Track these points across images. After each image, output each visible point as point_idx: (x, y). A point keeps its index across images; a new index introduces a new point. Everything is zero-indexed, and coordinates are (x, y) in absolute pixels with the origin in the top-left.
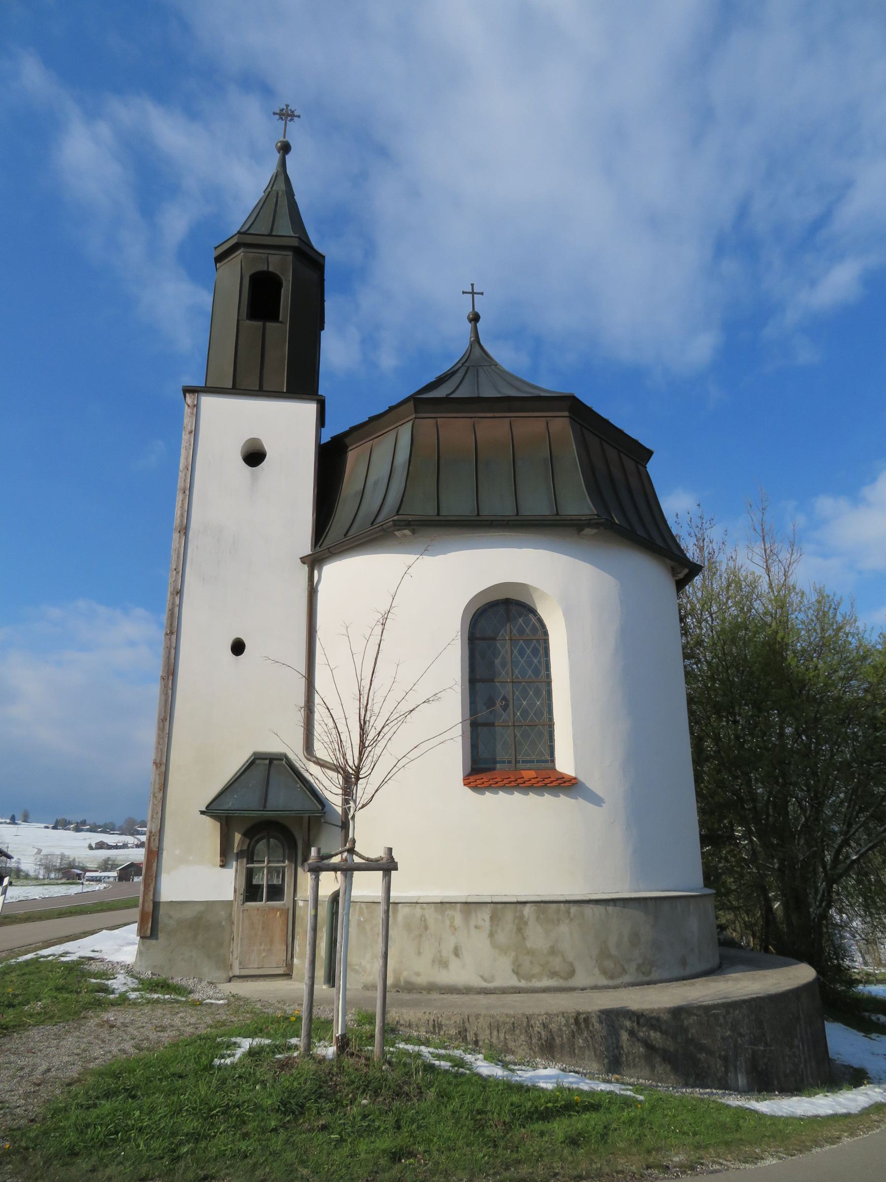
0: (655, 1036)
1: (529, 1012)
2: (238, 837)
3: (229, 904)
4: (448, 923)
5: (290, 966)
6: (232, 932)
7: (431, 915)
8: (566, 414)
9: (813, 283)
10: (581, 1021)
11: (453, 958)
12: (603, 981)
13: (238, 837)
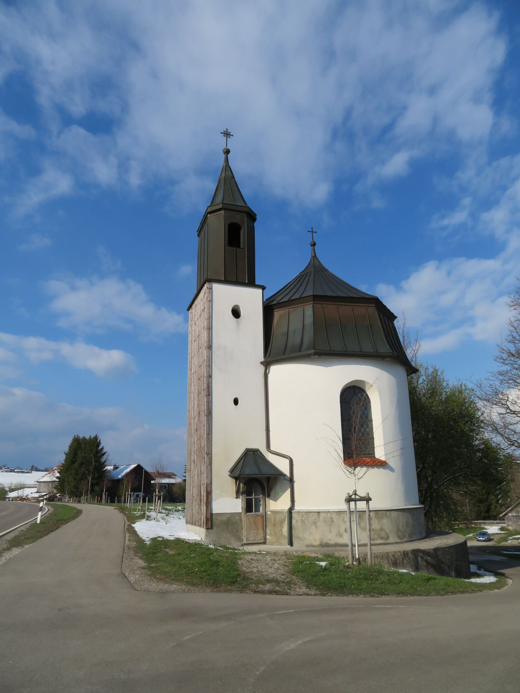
0: (429, 558)
1: (387, 551)
2: (242, 485)
3: (240, 514)
4: (342, 519)
5: (265, 539)
6: (242, 526)
7: (334, 516)
8: (374, 305)
9: (383, 162)
10: (405, 554)
11: (344, 533)
12: (399, 541)
13: (242, 485)
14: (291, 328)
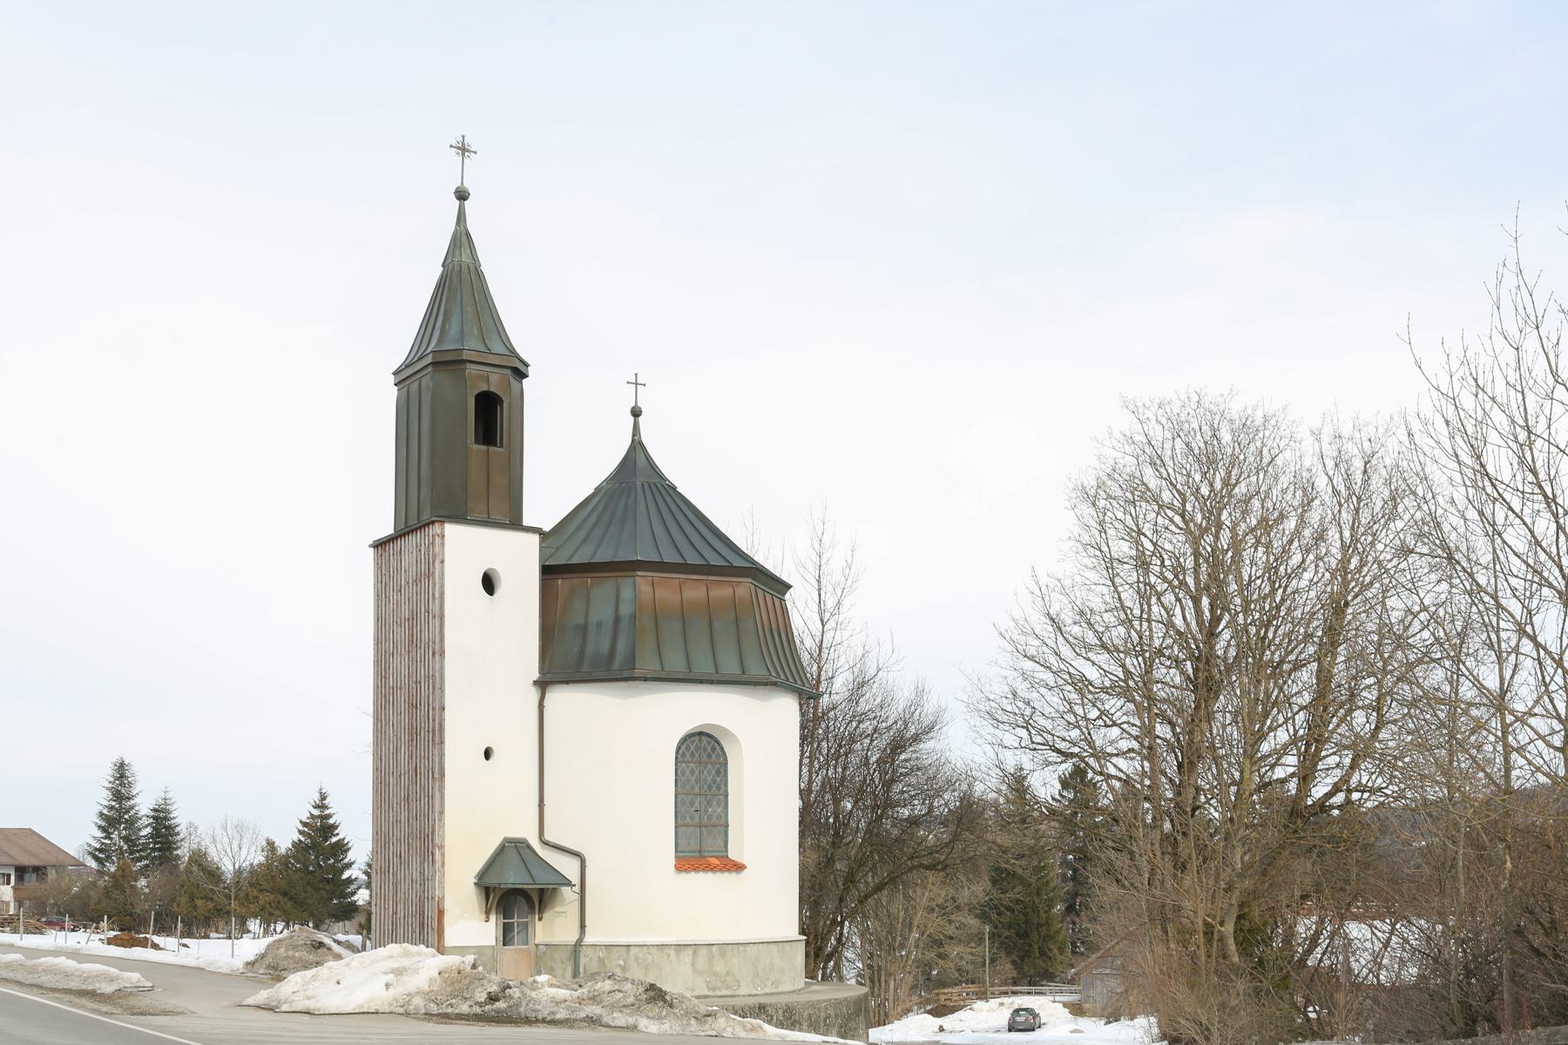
14: (593, 619)
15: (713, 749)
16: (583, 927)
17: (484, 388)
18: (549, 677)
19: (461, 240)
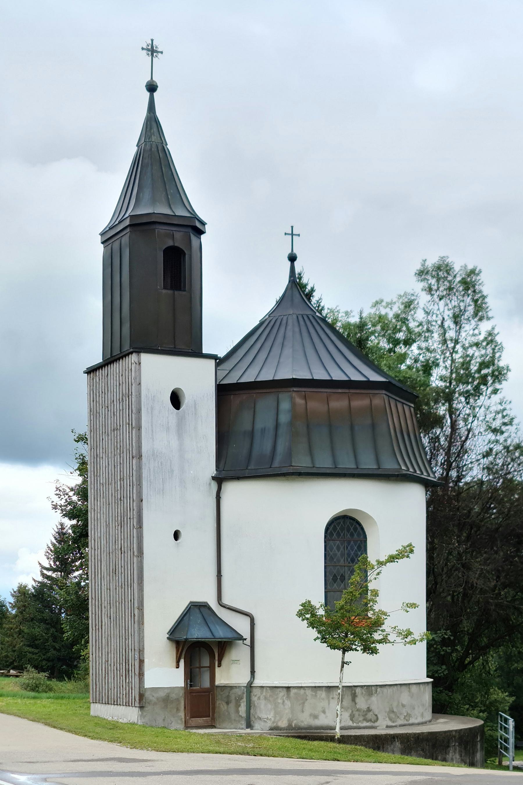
14: (259, 426)
15: (355, 529)
16: (253, 672)
17: (170, 243)
18: (223, 475)
19: (152, 123)
